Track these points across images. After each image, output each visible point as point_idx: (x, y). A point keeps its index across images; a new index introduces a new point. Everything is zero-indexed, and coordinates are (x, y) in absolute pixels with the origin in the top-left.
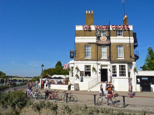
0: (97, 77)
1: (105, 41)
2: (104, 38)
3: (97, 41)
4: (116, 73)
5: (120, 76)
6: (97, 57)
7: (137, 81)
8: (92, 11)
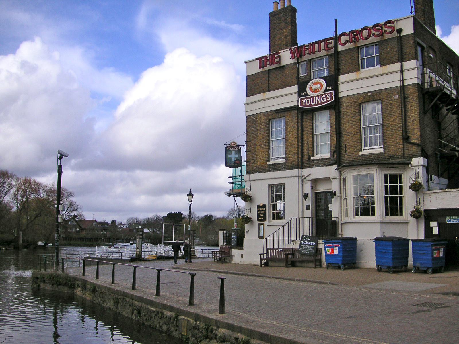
1: (321, 95)
6: (300, 156)
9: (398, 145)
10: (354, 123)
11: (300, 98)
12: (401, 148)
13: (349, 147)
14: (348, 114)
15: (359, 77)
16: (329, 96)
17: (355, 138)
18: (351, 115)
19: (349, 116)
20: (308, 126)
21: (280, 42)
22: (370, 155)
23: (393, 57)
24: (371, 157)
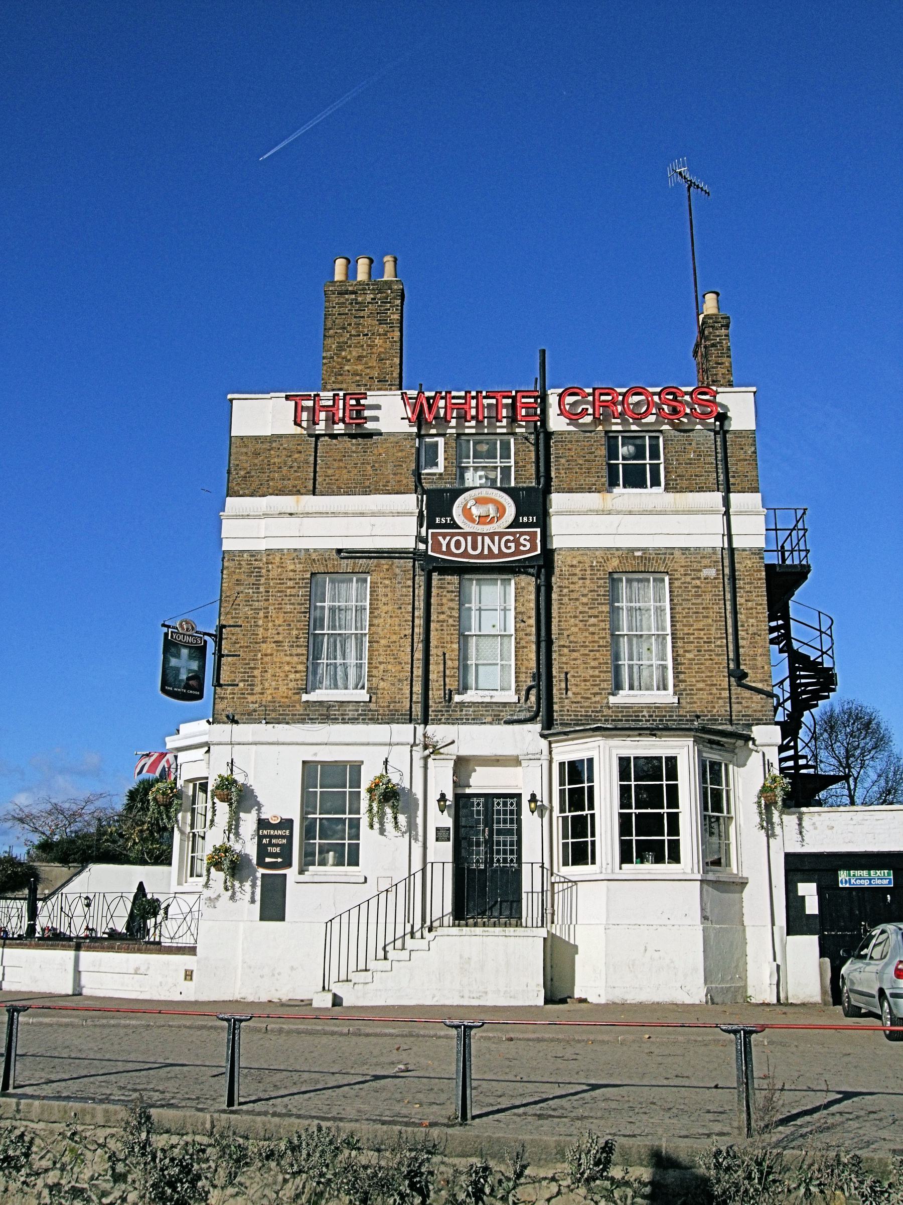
0: (417, 866)
1: (501, 535)
2: (492, 510)
3: (420, 539)
4: (591, 807)
5: (626, 858)
6: (418, 688)
7: (794, 903)
8: (388, 259)
9: (714, 691)
10: (593, 620)
11: (430, 531)
12: (725, 698)
13: (578, 679)
14: (574, 595)
15: (609, 506)
16: (525, 539)
17: (594, 659)
18: (585, 600)
19: (577, 599)
20: (445, 608)
21: (359, 367)
22: (641, 708)
23: (701, 476)
24: (642, 712)
